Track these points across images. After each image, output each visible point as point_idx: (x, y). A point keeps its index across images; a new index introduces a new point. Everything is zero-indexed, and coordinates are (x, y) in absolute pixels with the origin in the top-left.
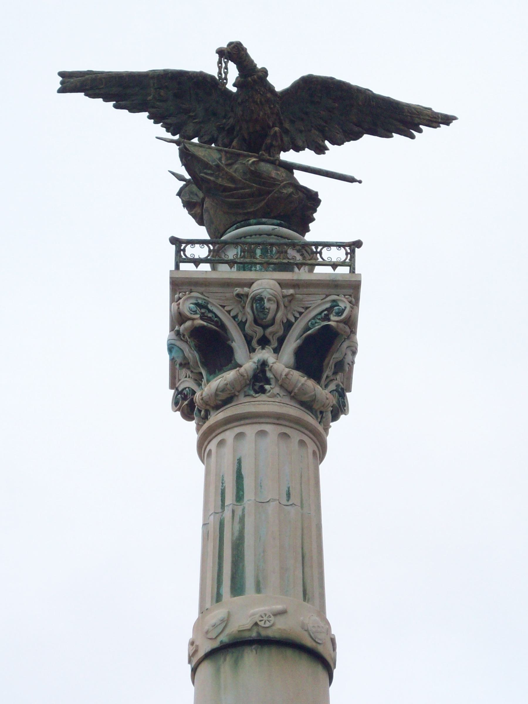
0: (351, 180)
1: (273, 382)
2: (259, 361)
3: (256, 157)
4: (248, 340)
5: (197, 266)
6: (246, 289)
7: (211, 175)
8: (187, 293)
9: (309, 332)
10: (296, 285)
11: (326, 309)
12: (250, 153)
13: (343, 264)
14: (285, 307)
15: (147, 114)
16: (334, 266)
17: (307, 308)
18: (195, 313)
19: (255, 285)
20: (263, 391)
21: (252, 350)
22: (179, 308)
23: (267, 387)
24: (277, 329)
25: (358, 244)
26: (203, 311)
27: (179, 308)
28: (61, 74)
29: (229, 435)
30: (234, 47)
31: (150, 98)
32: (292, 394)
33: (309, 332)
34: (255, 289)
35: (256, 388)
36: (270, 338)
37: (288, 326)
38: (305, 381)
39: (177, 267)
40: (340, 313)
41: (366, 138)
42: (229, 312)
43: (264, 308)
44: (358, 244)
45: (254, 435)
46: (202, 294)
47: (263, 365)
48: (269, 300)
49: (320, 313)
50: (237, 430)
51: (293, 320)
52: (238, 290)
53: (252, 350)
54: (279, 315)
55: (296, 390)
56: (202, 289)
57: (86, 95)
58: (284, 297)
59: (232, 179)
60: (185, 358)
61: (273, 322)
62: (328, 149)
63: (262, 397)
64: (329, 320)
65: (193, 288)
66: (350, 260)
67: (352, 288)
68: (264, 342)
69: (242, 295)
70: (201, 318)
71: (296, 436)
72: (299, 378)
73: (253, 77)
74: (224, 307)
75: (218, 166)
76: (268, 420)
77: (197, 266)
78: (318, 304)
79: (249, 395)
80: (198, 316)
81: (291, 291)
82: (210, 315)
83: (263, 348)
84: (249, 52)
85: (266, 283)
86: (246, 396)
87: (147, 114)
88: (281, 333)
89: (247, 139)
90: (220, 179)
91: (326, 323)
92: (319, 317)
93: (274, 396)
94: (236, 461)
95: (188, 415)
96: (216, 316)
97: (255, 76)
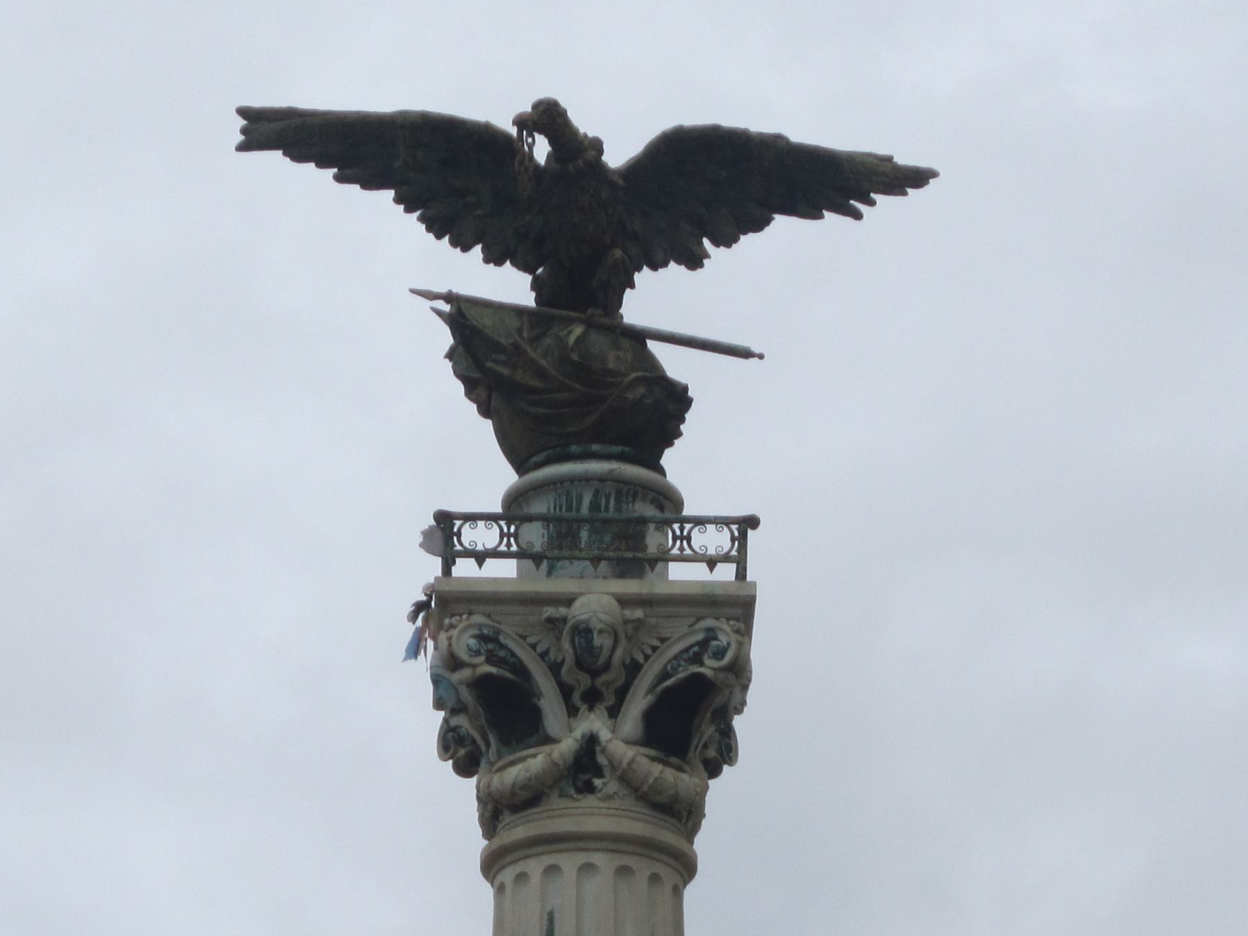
0: (744, 353)
1: (607, 771)
2: (583, 736)
3: (581, 321)
4: (566, 692)
5: (480, 564)
6: (563, 610)
7: (504, 363)
8: (464, 617)
9: (669, 683)
10: (646, 602)
11: (697, 644)
12: (572, 314)
13: (726, 558)
14: (629, 638)
15: (391, 193)
16: (712, 563)
17: (663, 640)
18: (477, 653)
19: (577, 604)
20: (589, 789)
21: (572, 711)
22: (450, 645)
23: (597, 782)
24: (615, 676)
25: (751, 522)
26: (491, 646)
27: (450, 645)
28: (243, 112)
29: (534, 867)
30: (544, 112)
31: (398, 164)
32: (640, 793)
33: (669, 683)
34: (580, 611)
35: (580, 784)
36: (604, 690)
37: (633, 669)
38: (662, 772)
39: (447, 570)
40: (720, 653)
41: (781, 223)
42: (534, 646)
43: (593, 647)
44: (751, 522)
45: (574, 872)
46: (489, 616)
47: (591, 741)
48: (601, 631)
49: (687, 650)
50: (548, 860)
51: (641, 659)
52: (549, 611)
53: (572, 711)
54: (618, 654)
55: (645, 788)
56: (488, 609)
57: (285, 154)
58: (626, 622)
59: (540, 373)
60: (459, 700)
61: (607, 667)
62: (708, 256)
63: (590, 801)
64: (702, 664)
65: (474, 607)
66: (739, 551)
67: (738, 607)
68: (592, 698)
69: (557, 620)
70: (489, 661)
71: (643, 868)
72: (653, 771)
73: (575, 150)
74: (524, 637)
75: (516, 346)
76: (598, 845)
77: (480, 564)
78: (683, 637)
79: (566, 796)
80: (482, 658)
81: (638, 613)
82: (502, 653)
83: (591, 709)
84: (569, 114)
85: (596, 597)
86: (561, 796)
87: (391, 193)
88: (620, 682)
89: (571, 251)
90: (520, 371)
91: (696, 669)
92: (685, 656)
93: (609, 798)
94: (546, 916)
95: (465, 768)
96: (513, 654)
97: (580, 162)
